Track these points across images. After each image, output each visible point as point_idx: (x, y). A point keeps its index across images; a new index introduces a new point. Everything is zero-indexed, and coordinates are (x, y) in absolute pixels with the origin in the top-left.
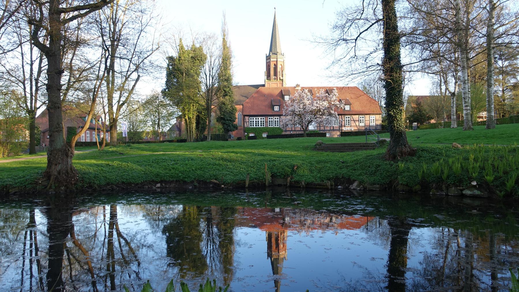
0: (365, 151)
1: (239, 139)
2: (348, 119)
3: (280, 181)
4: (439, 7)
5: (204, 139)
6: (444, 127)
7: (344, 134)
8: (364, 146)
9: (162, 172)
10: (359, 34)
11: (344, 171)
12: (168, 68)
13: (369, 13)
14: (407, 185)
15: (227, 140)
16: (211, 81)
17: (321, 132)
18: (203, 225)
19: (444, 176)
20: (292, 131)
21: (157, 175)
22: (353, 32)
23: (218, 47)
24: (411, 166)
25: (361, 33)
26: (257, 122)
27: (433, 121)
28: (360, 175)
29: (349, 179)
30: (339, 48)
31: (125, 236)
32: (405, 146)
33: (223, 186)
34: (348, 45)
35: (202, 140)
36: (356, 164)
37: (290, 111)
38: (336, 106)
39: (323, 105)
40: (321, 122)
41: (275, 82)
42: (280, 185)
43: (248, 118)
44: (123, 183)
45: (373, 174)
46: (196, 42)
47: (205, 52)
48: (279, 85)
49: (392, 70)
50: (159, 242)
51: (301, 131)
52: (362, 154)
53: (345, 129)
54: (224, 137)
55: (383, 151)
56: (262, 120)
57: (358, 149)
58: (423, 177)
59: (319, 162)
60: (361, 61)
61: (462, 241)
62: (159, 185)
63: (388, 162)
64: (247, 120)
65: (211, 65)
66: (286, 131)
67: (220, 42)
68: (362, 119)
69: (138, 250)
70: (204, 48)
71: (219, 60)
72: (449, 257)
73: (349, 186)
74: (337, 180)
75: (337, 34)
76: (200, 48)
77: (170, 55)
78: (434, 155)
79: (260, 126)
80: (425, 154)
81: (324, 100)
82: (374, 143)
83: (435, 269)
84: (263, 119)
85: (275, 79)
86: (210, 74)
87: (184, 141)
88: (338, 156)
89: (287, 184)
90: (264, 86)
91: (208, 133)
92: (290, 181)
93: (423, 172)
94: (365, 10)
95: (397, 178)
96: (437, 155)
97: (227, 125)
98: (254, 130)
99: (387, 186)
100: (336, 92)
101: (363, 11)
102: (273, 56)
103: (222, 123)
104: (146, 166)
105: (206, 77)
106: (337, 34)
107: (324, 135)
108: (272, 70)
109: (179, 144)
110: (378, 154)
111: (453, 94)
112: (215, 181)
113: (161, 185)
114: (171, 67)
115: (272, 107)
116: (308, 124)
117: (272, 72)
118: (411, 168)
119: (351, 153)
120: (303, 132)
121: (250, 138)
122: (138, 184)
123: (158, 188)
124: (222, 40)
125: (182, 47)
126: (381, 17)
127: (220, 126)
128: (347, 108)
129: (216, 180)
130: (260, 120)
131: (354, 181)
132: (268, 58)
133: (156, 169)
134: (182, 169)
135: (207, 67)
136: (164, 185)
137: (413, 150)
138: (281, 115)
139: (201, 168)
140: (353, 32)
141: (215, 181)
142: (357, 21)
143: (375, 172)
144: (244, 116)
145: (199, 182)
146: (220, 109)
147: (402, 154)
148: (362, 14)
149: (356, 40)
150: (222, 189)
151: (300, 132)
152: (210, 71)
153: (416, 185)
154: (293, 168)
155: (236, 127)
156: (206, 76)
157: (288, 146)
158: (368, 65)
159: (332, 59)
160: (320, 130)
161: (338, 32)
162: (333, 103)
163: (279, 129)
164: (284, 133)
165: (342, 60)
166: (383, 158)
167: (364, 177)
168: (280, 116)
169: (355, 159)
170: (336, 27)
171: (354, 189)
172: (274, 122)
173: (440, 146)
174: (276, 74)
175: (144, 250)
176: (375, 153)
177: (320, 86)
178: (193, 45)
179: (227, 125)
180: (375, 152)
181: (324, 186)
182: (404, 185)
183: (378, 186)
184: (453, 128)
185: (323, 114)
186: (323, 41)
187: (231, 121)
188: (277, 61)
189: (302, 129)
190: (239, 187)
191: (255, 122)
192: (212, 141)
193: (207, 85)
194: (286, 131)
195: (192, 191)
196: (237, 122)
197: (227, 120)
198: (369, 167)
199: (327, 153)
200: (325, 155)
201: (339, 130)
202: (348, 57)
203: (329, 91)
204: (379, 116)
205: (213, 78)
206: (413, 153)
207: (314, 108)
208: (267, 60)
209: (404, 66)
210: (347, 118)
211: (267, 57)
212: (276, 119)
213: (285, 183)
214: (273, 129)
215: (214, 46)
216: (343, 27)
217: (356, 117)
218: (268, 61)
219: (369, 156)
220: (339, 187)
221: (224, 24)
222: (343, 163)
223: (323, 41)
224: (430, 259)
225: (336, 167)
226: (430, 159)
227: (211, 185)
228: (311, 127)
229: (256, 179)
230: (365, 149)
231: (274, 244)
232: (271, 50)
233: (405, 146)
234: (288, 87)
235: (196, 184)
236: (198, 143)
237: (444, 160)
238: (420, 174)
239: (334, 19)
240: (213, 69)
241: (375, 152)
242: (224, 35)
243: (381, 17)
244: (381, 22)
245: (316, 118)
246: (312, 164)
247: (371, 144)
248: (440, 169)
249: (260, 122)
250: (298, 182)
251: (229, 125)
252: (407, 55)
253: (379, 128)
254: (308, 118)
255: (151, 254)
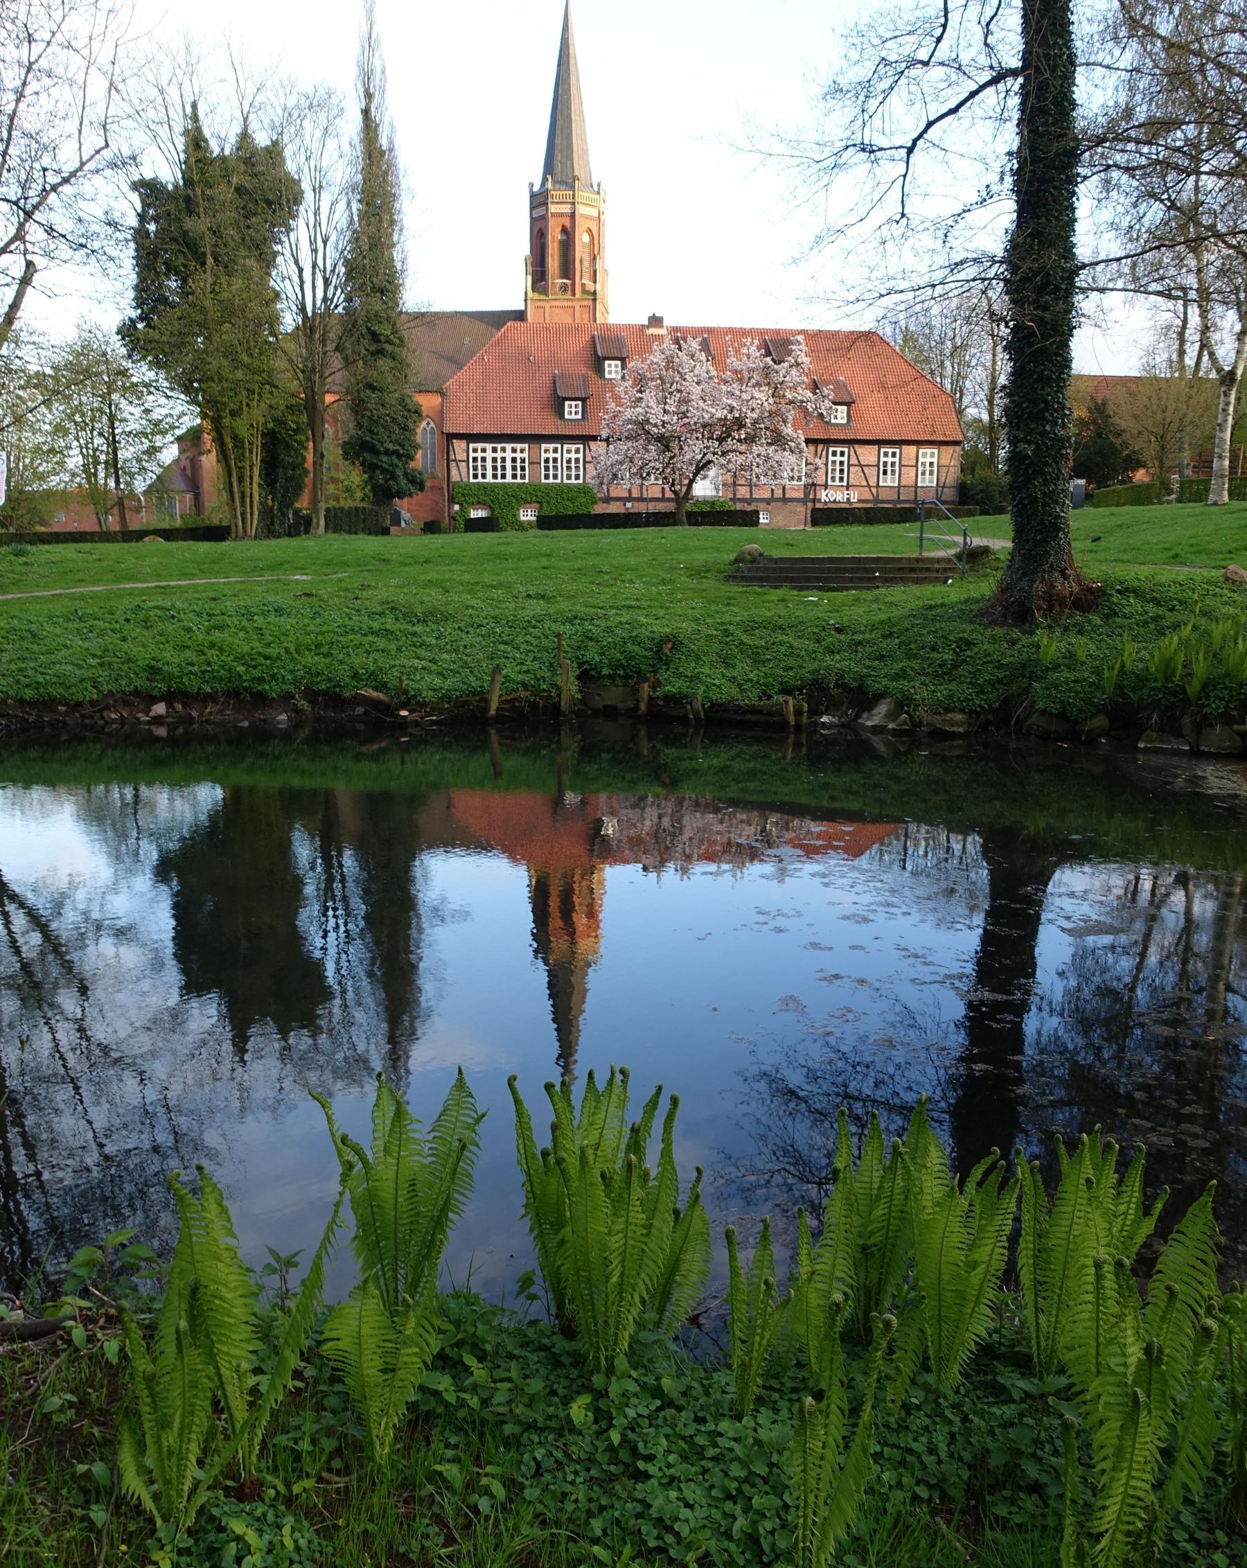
0: (915, 590)
1: (431, 527)
2: (838, 458)
3: (612, 695)
4: (1221, 21)
5: (302, 526)
6: (1179, 501)
7: (825, 516)
8: (912, 570)
9: (171, 658)
10: (923, 126)
11: (837, 662)
12: (140, 235)
13: (964, 39)
14: (1062, 715)
15: (385, 532)
16: (320, 294)
17: (739, 506)
18: (304, 850)
19: (1193, 688)
20: (630, 499)
21: (153, 671)
22: (899, 118)
23: (346, 147)
24: (1085, 647)
25: (930, 124)
26: (491, 465)
27: (1140, 476)
28: (902, 675)
29: (861, 689)
30: (841, 178)
31: (31, 898)
32: (1063, 572)
33: (404, 713)
34: (878, 170)
35: (292, 532)
36: (885, 636)
37: (629, 421)
38: (801, 406)
39: (753, 403)
40: (743, 468)
41: (562, 300)
42: (610, 712)
43: (463, 444)
44: (21, 702)
45: (945, 673)
46: (254, 126)
47: (291, 166)
48: (581, 317)
49: (1040, 279)
50: (151, 910)
51: (663, 499)
52: (906, 598)
53: (833, 496)
54: (372, 519)
55: (984, 587)
56: (518, 455)
57: (888, 581)
58: (1119, 687)
59: (751, 627)
60: (928, 240)
61: (1204, 908)
62: (160, 709)
63: (999, 631)
64: (461, 456)
65: (317, 223)
66: (608, 500)
67: (351, 126)
68: (890, 459)
69: (84, 947)
70: (288, 153)
71: (349, 203)
72: (1153, 959)
73: (858, 716)
74: (818, 693)
75: (838, 122)
76: (274, 152)
77: (148, 175)
78: (1163, 607)
79: (509, 479)
80: (1134, 605)
81: (758, 384)
82: (948, 560)
83: (1104, 991)
84: (523, 451)
85: (564, 288)
86: (314, 265)
87: (217, 534)
88: (814, 604)
89: (637, 707)
90: (520, 316)
91: (314, 502)
92: (650, 698)
93: (1123, 666)
94: (954, 17)
95: (1027, 690)
96: (1172, 609)
97: (384, 471)
98: (485, 495)
99: (991, 717)
100: (801, 352)
101: (944, 26)
102: (557, 193)
103: (362, 464)
104: (101, 634)
105: (302, 271)
106: (838, 122)
107: (750, 519)
108: (556, 252)
109: (204, 547)
110: (967, 601)
111: (1228, 378)
112: (374, 694)
113: (170, 706)
114: (152, 227)
115: (557, 405)
116: (695, 475)
117: (553, 263)
118: (1082, 655)
119: (868, 595)
120: (670, 507)
121: (474, 526)
122: (79, 705)
123: (158, 720)
124: (359, 117)
125: (196, 141)
126: (1015, 63)
127: (355, 477)
128: (840, 415)
129: (375, 689)
130: (489, 455)
131: (879, 697)
132: (539, 200)
133: (143, 648)
134: (246, 648)
135: (301, 231)
136: (179, 707)
137: (1090, 590)
138: (594, 438)
139: (319, 646)
140: (899, 118)
141: (374, 694)
142: (917, 71)
143: (955, 666)
144: (451, 437)
145: (312, 695)
146: (358, 406)
147: (1053, 602)
148: (939, 40)
149: (910, 150)
150: (403, 724)
151: (661, 507)
152: (315, 251)
153: (1093, 716)
154: (660, 649)
155: (417, 483)
156: (301, 270)
157: (632, 561)
158: (957, 258)
159: (817, 227)
160: (734, 500)
161: (846, 111)
162: (789, 395)
163: (584, 490)
164: (599, 509)
165: (850, 232)
166: (985, 614)
167: (920, 690)
168: (586, 439)
169: (884, 617)
170: (837, 90)
171: (877, 730)
172: (564, 466)
173: (1182, 573)
174: (567, 269)
175: (107, 946)
176: (954, 598)
177: (747, 326)
178: (245, 136)
179: (384, 471)
180: (953, 592)
181: (771, 714)
182: (1051, 714)
183: (959, 717)
184: (1215, 504)
185: (751, 439)
186: (781, 148)
187: (399, 456)
188: (573, 215)
189: (669, 494)
190: (466, 722)
191: (489, 464)
192: (331, 536)
193: (302, 309)
194: (608, 500)
195: (287, 736)
196: (419, 461)
197: (387, 452)
198: (934, 648)
199: (780, 593)
200: (774, 603)
201: (804, 501)
202: (878, 217)
203: (776, 346)
204: (951, 449)
205: (327, 283)
206: (1090, 599)
207: (719, 415)
208: (532, 208)
209: (1084, 266)
210: (838, 455)
211: (533, 196)
212: (572, 451)
213: (631, 704)
214: (562, 490)
215: (331, 144)
216: (865, 89)
217: (868, 454)
218: (539, 212)
219: (931, 608)
220: (824, 719)
221: (370, 43)
222: (839, 630)
223: (781, 148)
224: (1089, 962)
225: (812, 646)
226: (1146, 623)
227: (360, 710)
228: (703, 489)
229: (525, 686)
230: (918, 581)
231: (559, 914)
232: (549, 168)
233: (1063, 572)
234: (619, 326)
235: (303, 704)
236: (273, 542)
237: (1195, 628)
238: (1110, 675)
239: (834, 60)
240: (325, 243)
241: (953, 592)
242: (369, 96)
243: (1015, 63)
244: (1016, 84)
245: (724, 454)
246: (727, 633)
247: (939, 560)
248: (1181, 658)
249: (509, 464)
250: (675, 700)
251: (393, 476)
252: (1100, 220)
253: (949, 494)
254: (695, 449)
255: (131, 956)
